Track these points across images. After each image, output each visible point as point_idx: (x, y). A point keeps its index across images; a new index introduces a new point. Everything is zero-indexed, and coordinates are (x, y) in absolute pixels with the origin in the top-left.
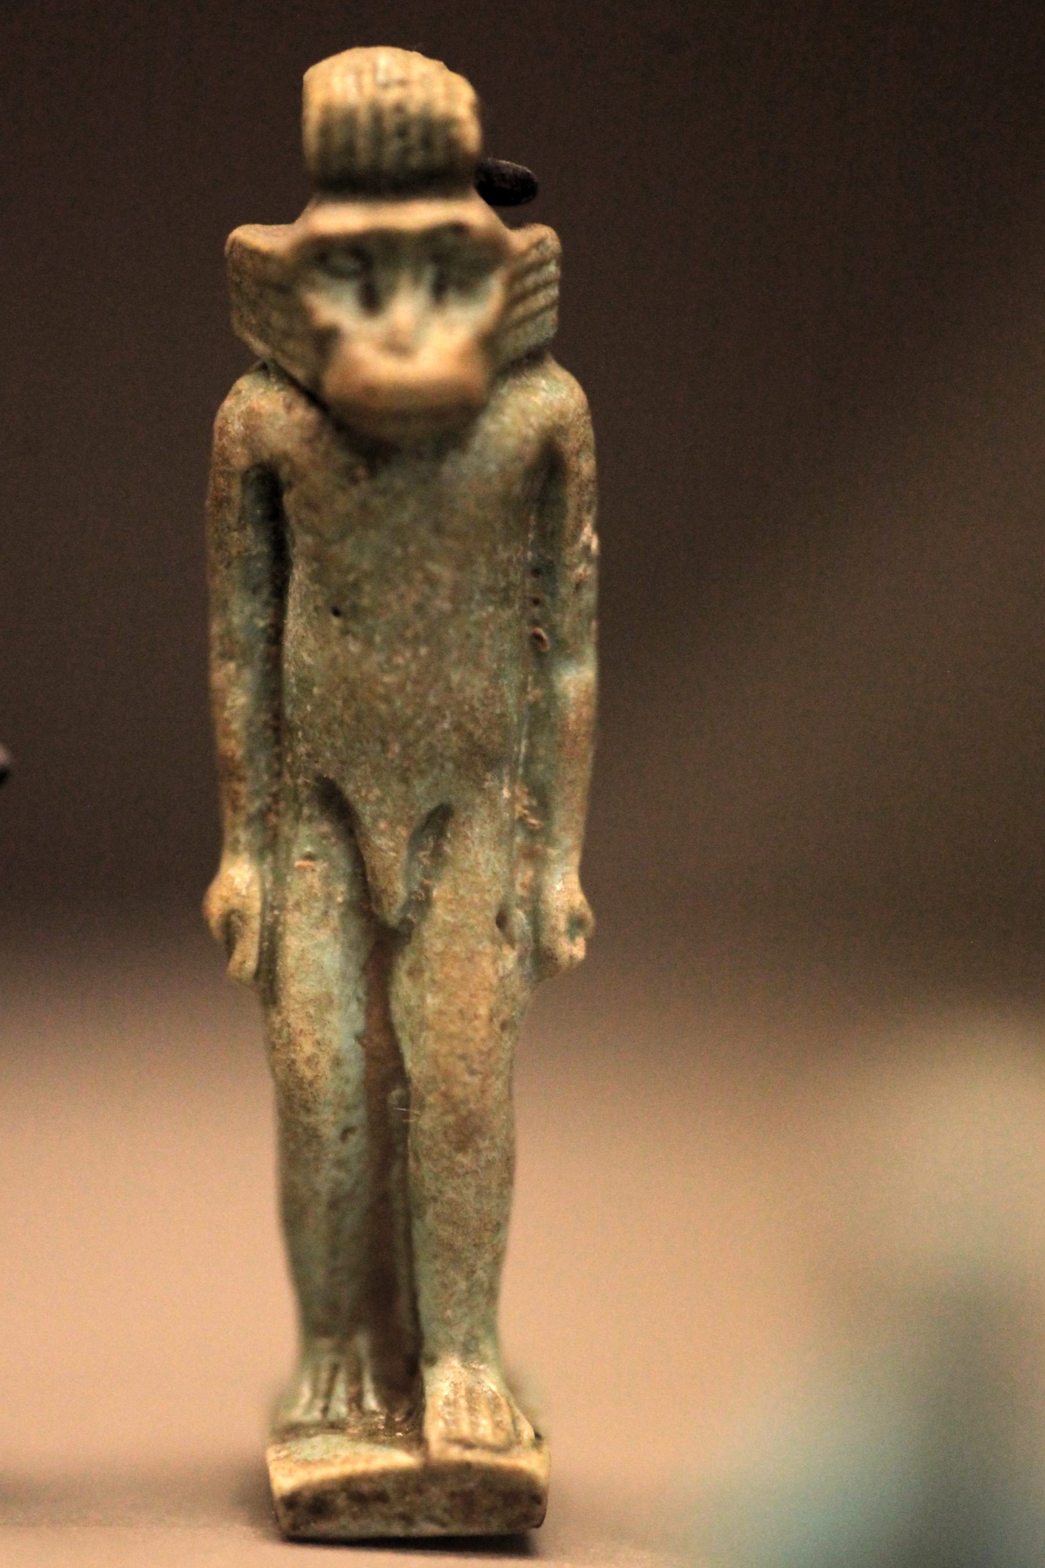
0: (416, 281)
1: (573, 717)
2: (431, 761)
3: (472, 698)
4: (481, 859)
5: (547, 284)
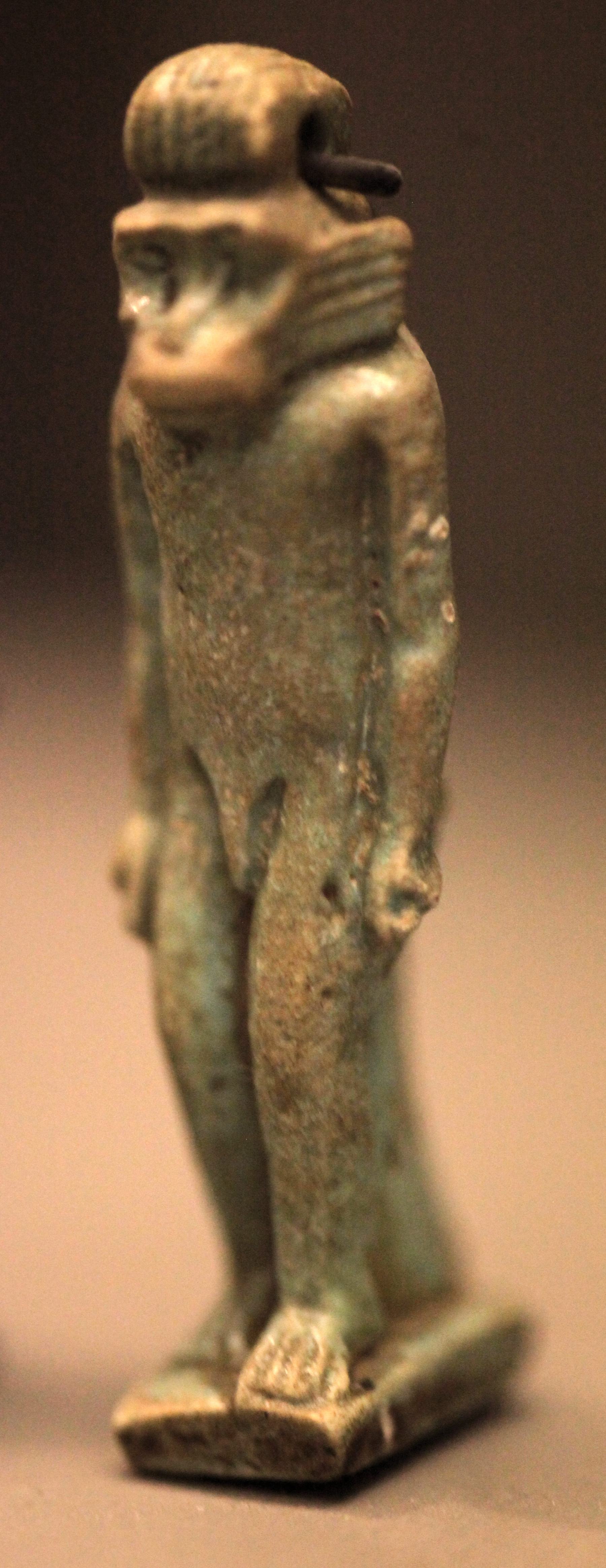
0: (207, 276)
1: (404, 697)
2: (259, 734)
3: (292, 677)
4: (310, 833)
5: (374, 279)
